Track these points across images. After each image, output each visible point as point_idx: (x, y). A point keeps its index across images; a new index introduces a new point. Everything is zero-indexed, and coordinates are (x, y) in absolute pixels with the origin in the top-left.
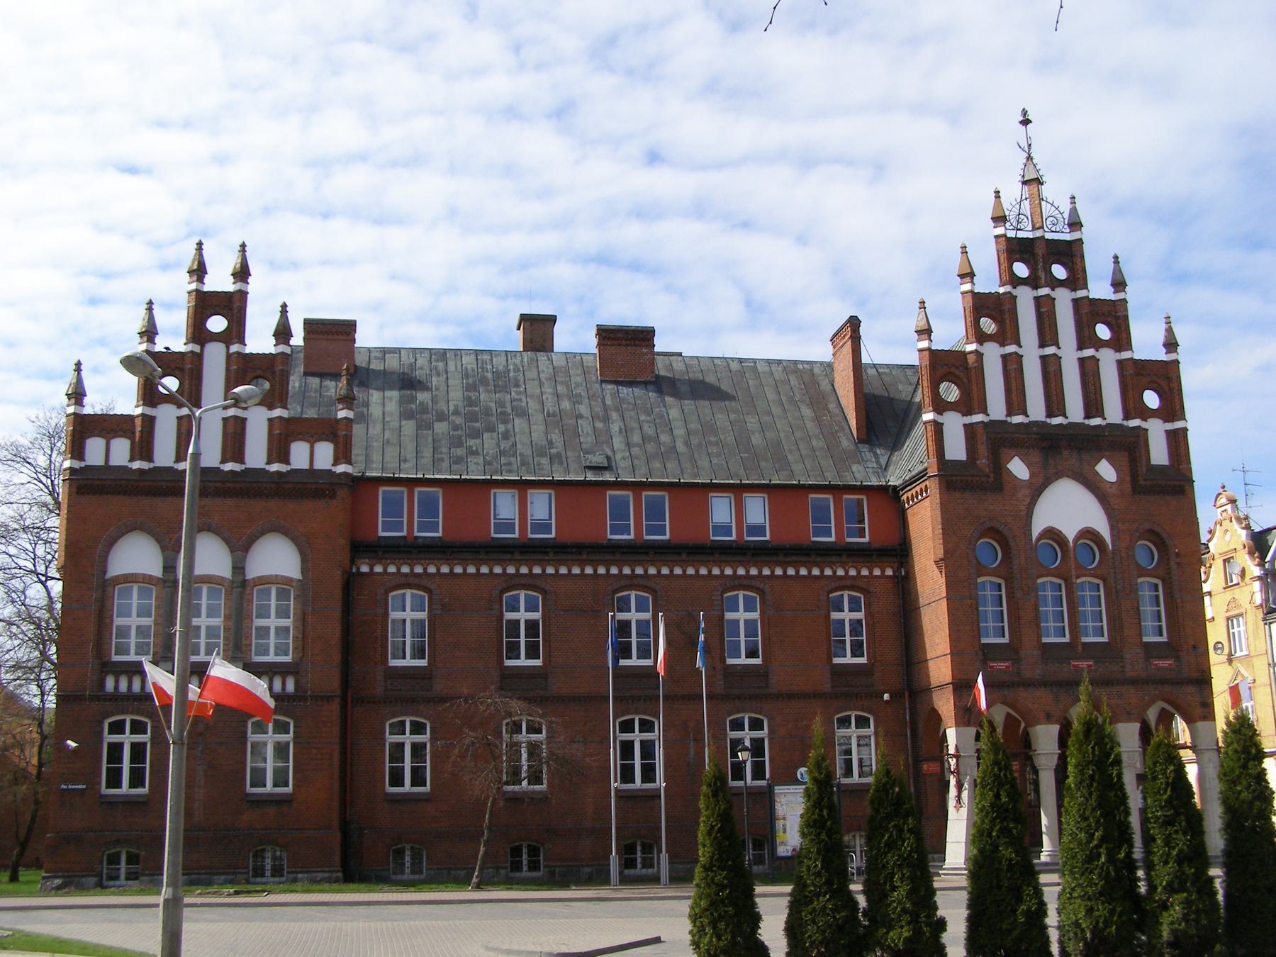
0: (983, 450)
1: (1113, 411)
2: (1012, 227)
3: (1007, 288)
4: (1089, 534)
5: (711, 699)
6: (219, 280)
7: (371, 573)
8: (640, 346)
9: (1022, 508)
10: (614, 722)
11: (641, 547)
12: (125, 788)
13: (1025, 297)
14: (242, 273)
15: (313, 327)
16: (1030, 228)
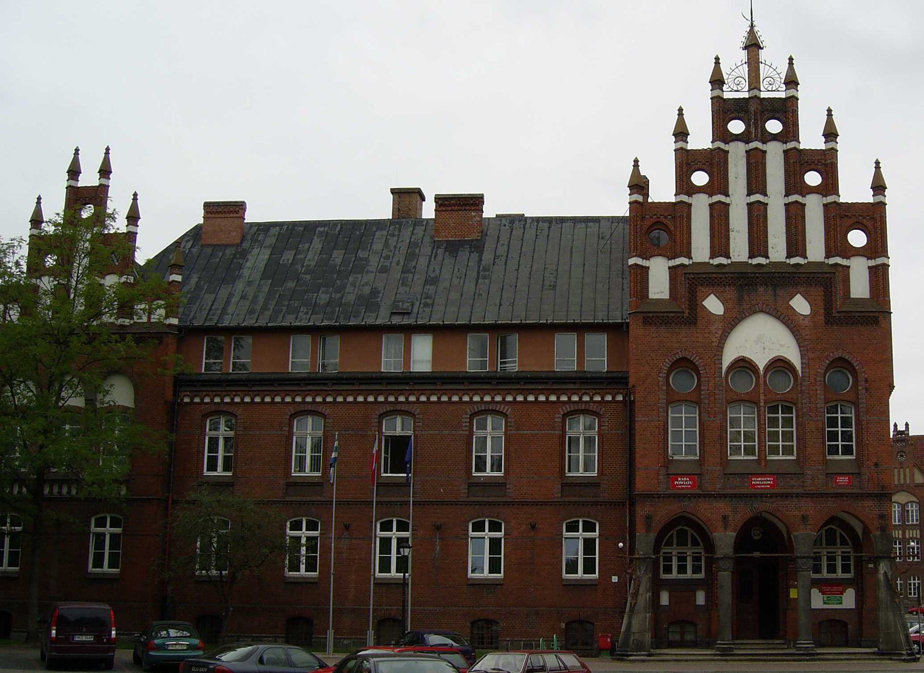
0: (683, 290)
1: (816, 250)
2: (730, 89)
3: (719, 144)
4: (779, 365)
5: (415, 505)
6: (89, 178)
7: (192, 402)
8: (469, 210)
9: (715, 340)
10: (376, 522)
11: (376, 378)
12: (580, 574)
13: (737, 154)
14: (105, 171)
15: (443, 202)
16: (747, 89)
